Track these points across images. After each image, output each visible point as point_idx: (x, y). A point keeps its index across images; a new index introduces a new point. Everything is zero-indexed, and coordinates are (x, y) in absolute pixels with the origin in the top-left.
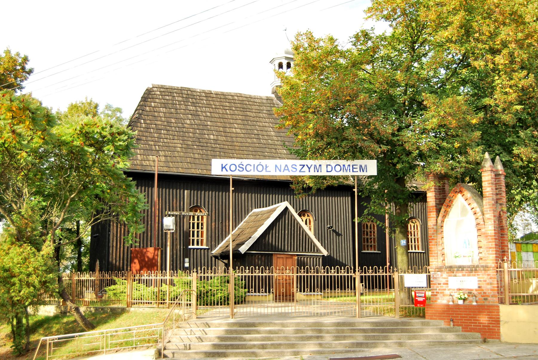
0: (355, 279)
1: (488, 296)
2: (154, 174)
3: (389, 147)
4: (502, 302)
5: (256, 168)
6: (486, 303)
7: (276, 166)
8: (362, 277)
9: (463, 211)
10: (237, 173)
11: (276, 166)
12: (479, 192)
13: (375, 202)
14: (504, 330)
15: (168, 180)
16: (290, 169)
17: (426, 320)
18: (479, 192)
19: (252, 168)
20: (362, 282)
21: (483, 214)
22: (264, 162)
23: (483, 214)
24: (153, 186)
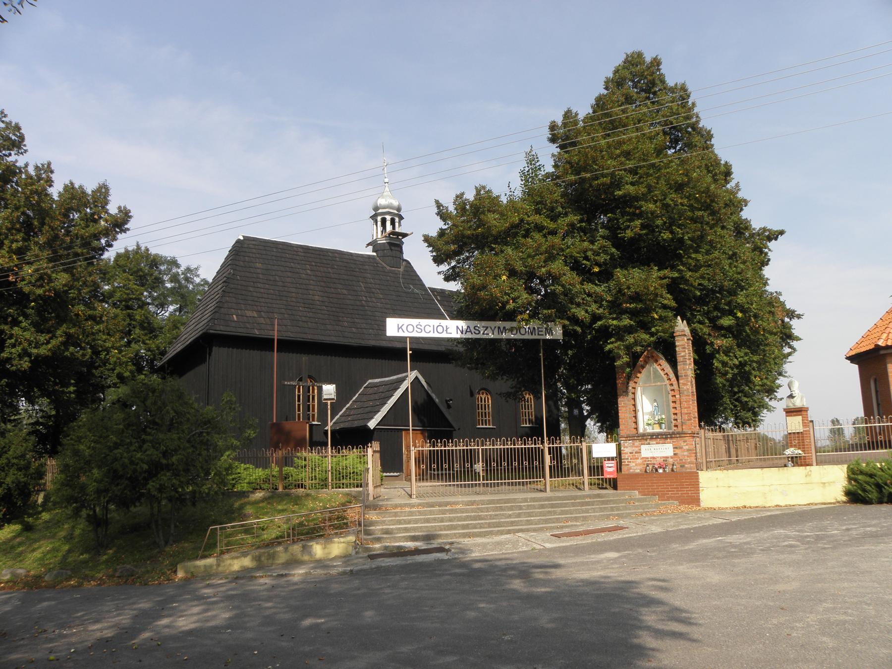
0: (542, 450)
1: (685, 463)
2: (273, 340)
3: (632, 323)
4: (699, 468)
5: (435, 329)
6: (684, 470)
7: (457, 327)
8: (549, 448)
9: (797, 427)
10: (415, 334)
11: (457, 327)
12: (673, 361)
13: (676, 426)
14: (703, 496)
15: (287, 346)
16: (473, 330)
17: (619, 491)
18: (673, 361)
19: (431, 329)
20: (550, 454)
21: (678, 380)
22: (444, 323)
23: (678, 380)
24: (273, 351)
